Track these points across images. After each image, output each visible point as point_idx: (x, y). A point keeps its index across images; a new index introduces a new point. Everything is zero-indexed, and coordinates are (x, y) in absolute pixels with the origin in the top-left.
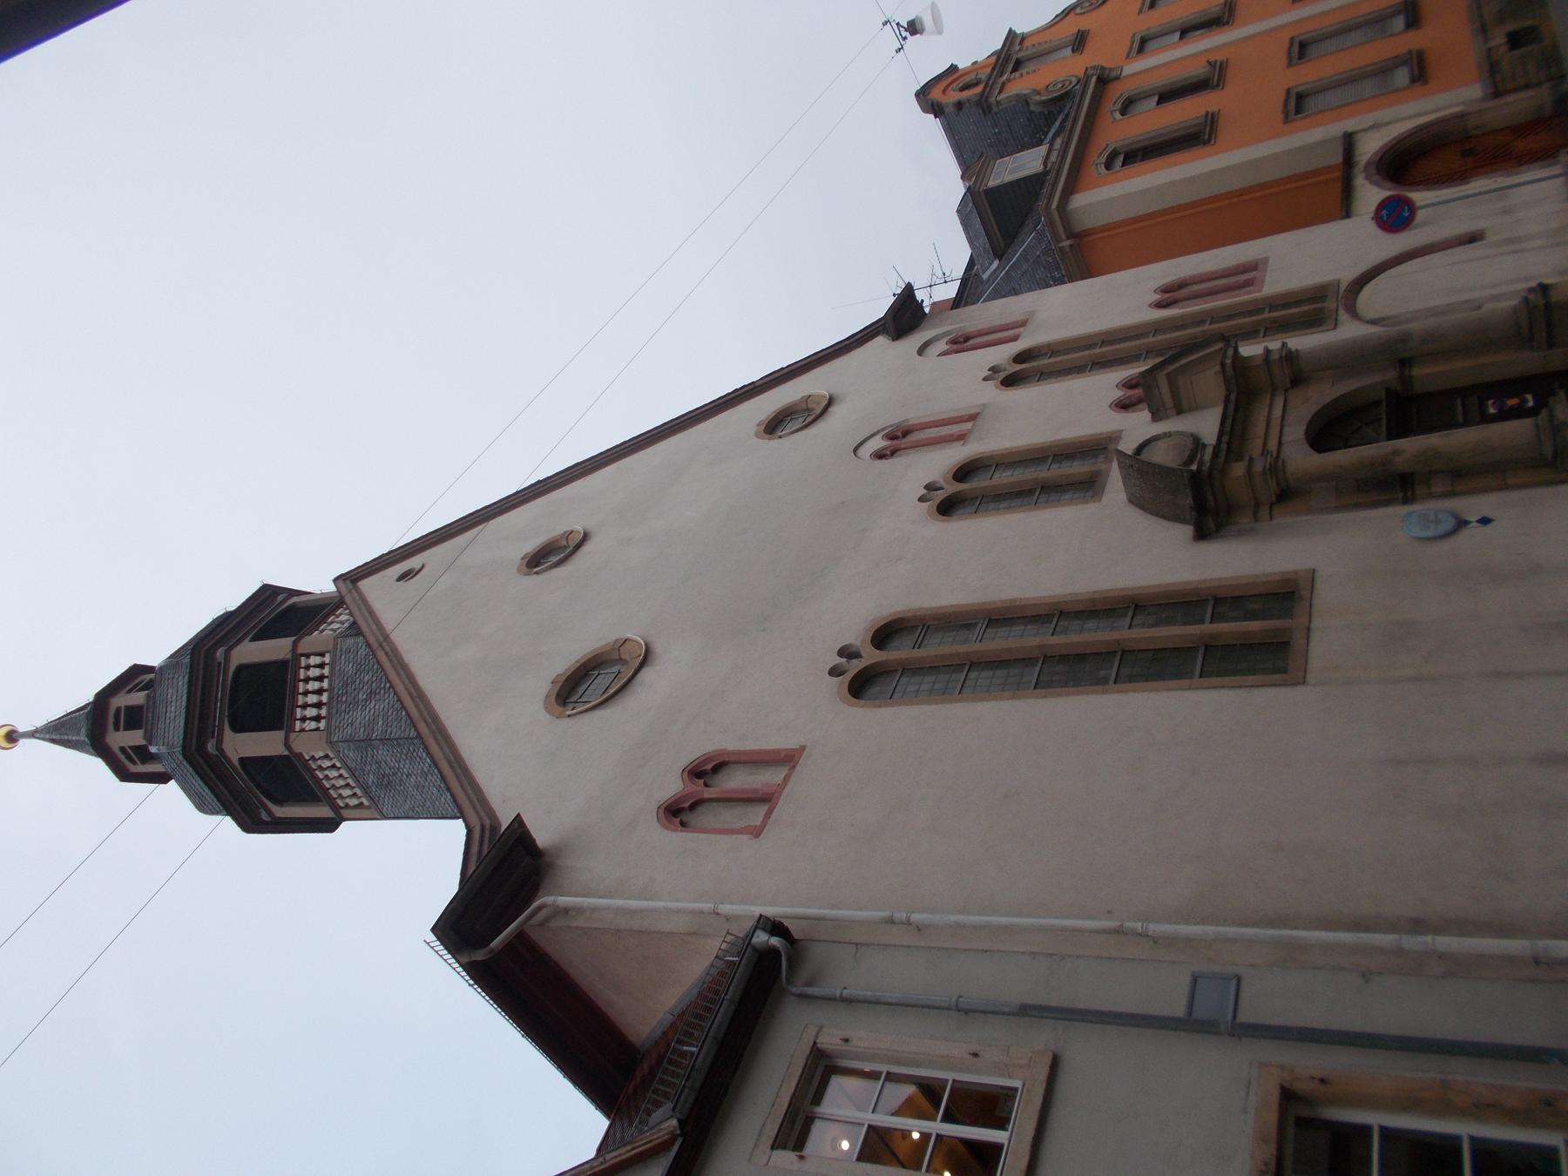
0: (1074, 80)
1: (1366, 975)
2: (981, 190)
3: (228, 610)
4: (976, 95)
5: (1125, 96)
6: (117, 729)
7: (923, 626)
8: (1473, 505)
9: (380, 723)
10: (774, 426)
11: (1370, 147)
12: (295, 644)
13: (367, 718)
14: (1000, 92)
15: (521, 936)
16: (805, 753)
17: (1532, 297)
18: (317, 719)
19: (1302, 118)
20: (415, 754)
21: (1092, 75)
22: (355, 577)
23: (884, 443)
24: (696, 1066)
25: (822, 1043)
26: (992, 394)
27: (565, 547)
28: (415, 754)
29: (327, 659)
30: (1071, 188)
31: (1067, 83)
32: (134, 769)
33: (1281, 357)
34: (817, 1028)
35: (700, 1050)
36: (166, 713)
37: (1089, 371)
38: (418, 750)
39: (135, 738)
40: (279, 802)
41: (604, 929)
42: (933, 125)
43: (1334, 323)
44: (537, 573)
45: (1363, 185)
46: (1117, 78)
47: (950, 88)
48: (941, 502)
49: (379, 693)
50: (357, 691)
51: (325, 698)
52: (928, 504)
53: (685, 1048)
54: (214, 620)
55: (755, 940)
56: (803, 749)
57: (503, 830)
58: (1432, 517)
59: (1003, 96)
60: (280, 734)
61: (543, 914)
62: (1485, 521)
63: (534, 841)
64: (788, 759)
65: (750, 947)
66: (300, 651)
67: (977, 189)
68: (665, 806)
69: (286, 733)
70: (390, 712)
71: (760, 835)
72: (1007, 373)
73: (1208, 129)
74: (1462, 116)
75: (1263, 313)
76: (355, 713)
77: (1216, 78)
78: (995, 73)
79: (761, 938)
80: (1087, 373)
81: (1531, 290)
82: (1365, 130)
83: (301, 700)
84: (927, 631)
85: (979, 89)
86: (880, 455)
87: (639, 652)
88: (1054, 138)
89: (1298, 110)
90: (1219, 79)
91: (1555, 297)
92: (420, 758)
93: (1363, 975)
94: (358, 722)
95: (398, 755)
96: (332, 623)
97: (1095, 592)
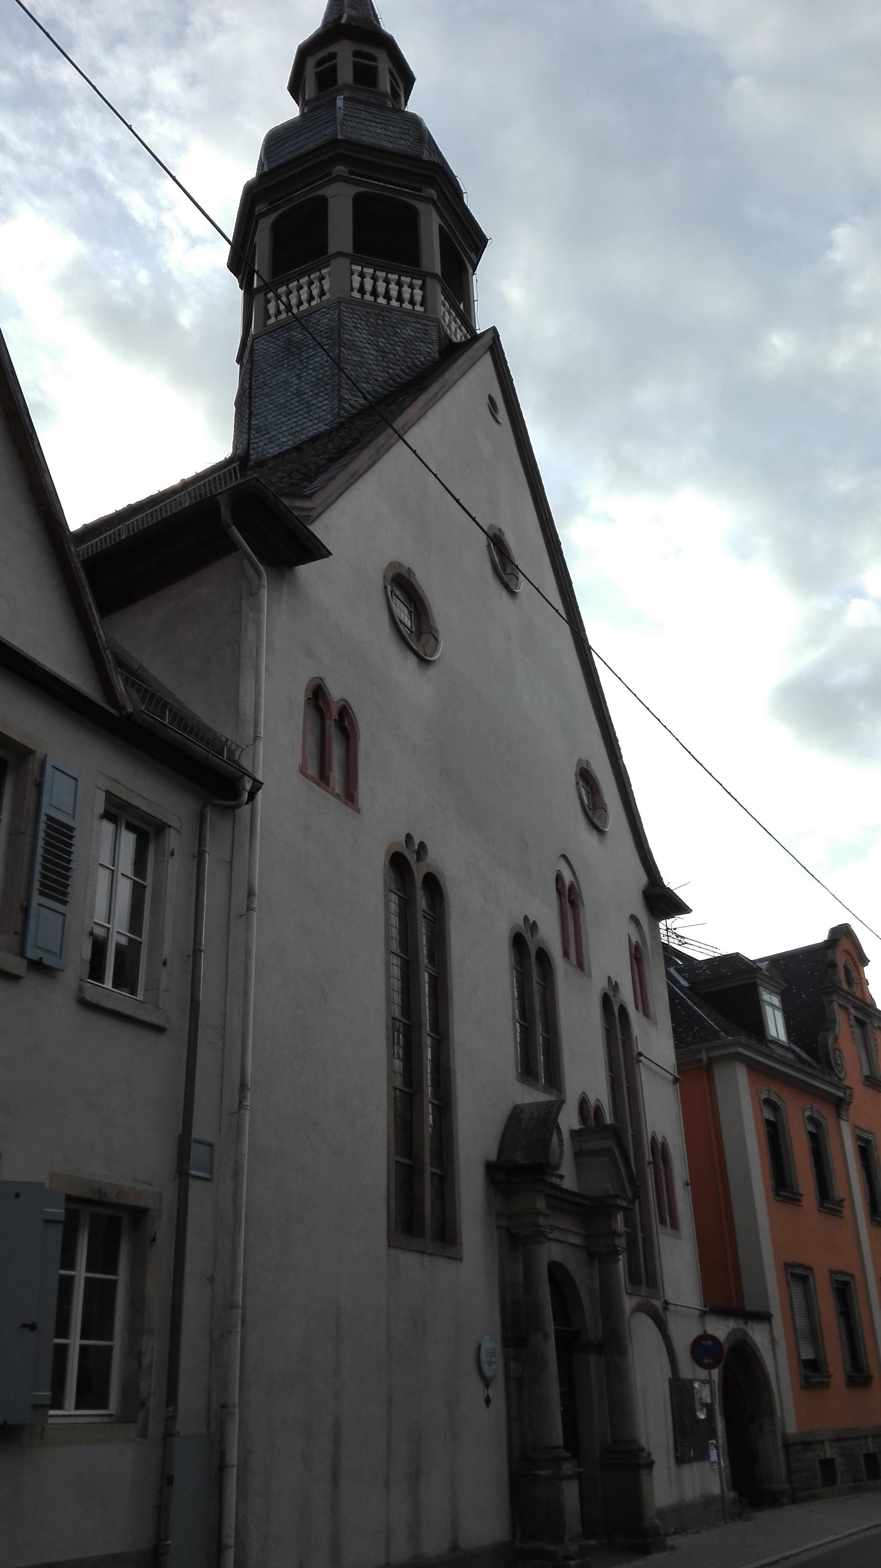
0: (842, 1076)
1: (211, 1279)
2: (757, 980)
3: (465, 195)
4: (840, 982)
5: (823, 1122)
6: (357, 54)
7: (435, 918)
8: (498, 1393)
9: (355, 358)
10: (586, 776)
11: (758, 1335)
12: (434, 276)
13: (360, 344)
14: (840, 1005)
15: (232, 547)
16: (355, 813)
17: (644, 1455)
18: (362, 290)
19: (787, 1280)
20: (322, 389)
21: (845, 1093)
22: (495, 350)
23: (567, 883)
24: (169, 730)
25: (170, 833)
26: (599, 984)
27: (504, 571)
28: (322, 389)
29: (418, 308)
30: (753, 1067)
31: (840, 1069)
32: (311, 62)
33: (617, 1246)
34: (178, 828)
35: (224, 761)
36: (375, 122)
37: (610, 1075)
38: (326, 394)
39: (345, 74)
40: (275, 228)
41: (241, 631)
42: (821, 937)
43: (631, 1292)
44: (489, 546)
45: (728, 1327)
46: (839, 1116)
47: (848, 958)
48: (523, 936)
49: (383, 361)
50: (386, 336)
51: (381, 301)
52: (523, 925)
53: (167, 712)
54: (454, 177)
55: (246, 778)
56: (358, 811)
57: (308, 526)
58: (493, 1359)
59: (836, 1007)
60: (349, 248)
61: (251, 572)
62: (488, 1401)
63: (304, 564)
64: (350, 796)
65: (240, 774)
66: (429, 281)
67: (758, 976)
68: (323, 685)
69: (350, 254)
70: (366, 371)
71: (302, 774)
72: (612, 998)
73: (788, 1194)
74: (772, 1414)
75: (643, 1232)
76: (365, 332)
77: (829, 1206)
78: (857, 1002)
79: (248, 785)
80: (608, 1073)
81: (649, 1454)
82: (771, 1332)
83: (381, 274)
84: (431, 920)
85: (845, 986)
86: (559, 878)
87: (428, 653)
88: (793, 1051)
89: (794, 1275)
90: (828, 1208)
91: (644, 1472)
92: (317, 394)
93: (212, 1277)
94: (357, 334)
95: (322, 371)
96: (450, 314)
97: (455, 1072)
